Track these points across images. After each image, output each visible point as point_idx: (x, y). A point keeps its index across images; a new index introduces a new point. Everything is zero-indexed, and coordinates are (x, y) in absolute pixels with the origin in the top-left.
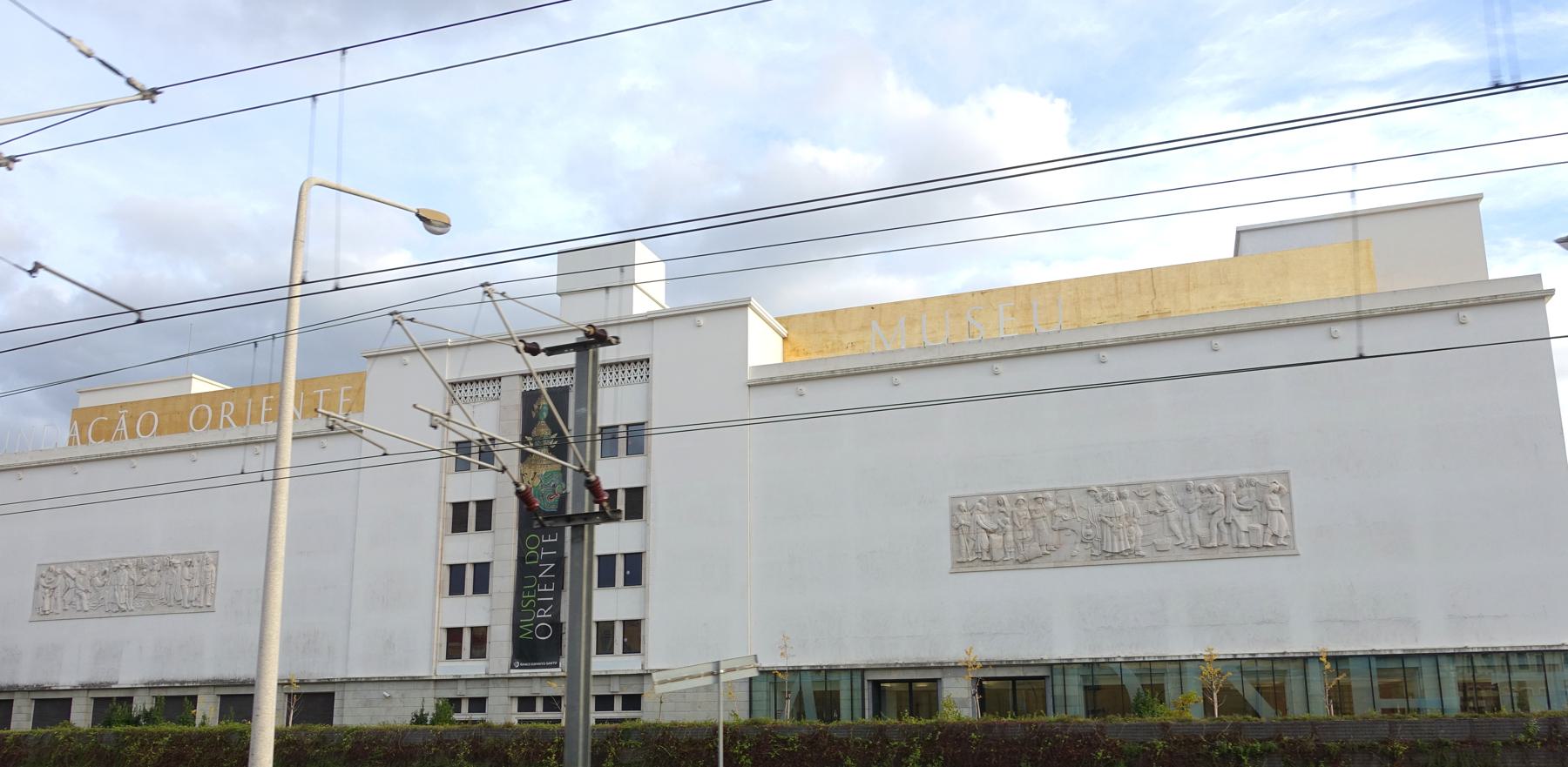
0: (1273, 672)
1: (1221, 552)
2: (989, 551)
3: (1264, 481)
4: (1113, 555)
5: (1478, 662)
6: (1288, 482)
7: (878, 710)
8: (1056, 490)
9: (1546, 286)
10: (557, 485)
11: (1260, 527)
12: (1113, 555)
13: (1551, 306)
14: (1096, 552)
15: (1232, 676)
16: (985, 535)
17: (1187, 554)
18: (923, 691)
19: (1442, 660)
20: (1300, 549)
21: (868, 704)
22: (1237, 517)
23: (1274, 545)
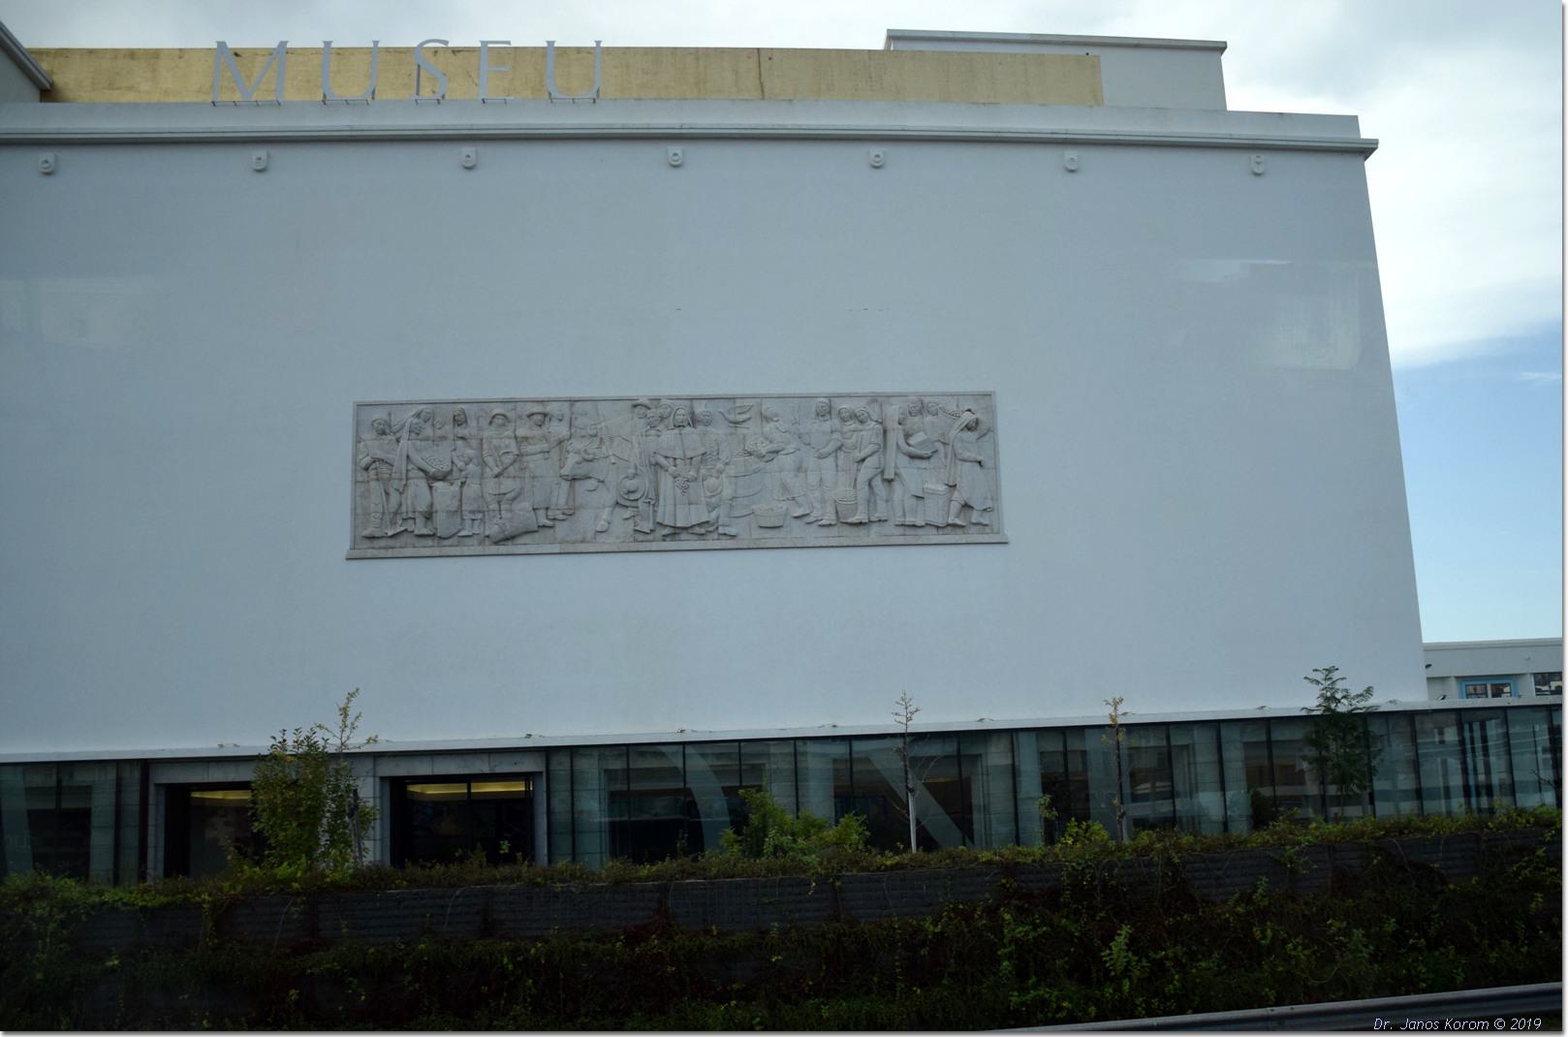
0: (1269, 743)
1: (874, 534)
2: (429, 516)
3: (952, 408)
4: (676, 532)
5: (689, 750)
6: (991, 410)
7: (178, 862)
8: (572, 402)
9: (1366, 133)
10: (376, 43)
11: (942, 488)
12: (676, 532)
13: (1371, 164)
14: (646, 526)
15: (889, 765)
16: (423, 484)
17: (813, 535)
18: (441, 805)
19: (1417, 718)
20: (1009, 531)
21: (156, 837)
22: (918, 473)
23: (970, 522)
